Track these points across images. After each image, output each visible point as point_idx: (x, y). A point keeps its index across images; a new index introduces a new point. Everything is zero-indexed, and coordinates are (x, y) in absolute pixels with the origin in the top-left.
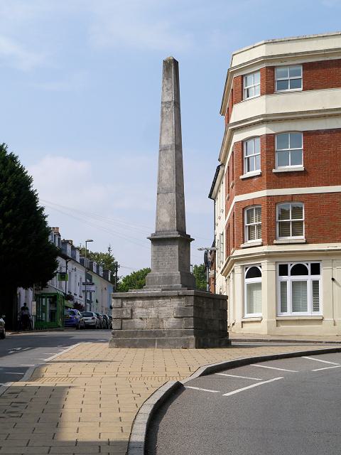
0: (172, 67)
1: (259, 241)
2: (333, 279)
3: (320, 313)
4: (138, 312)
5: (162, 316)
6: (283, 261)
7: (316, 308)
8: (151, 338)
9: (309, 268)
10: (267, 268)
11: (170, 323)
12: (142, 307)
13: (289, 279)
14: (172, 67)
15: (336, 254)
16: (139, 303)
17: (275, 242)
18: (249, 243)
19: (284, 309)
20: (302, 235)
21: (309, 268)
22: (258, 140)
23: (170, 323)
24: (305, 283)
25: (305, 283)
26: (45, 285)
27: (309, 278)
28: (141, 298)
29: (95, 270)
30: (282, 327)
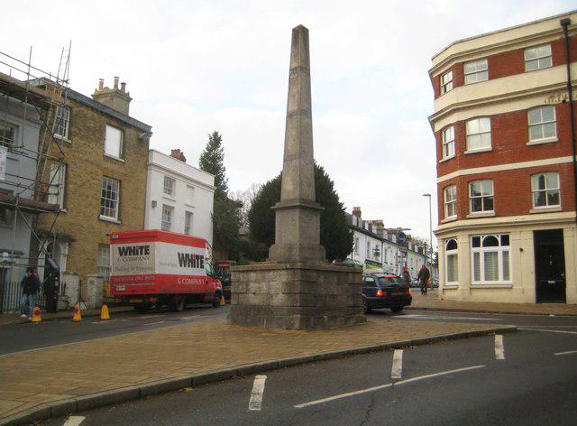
0: (301, 36)
2: (521, 250)
3: (510, 282)
4: (253, 286)
5: (272, 292)
7: (506, 276)
9: (499, 239)
10: (463, 241)
11: (279, 299)
12: (255, 282)
13: (482, 250)
14: (301, 36)
15: (570, 223)
16: (253, 275)
17: (468, 216)
18: (448, 218)
19: (477, 278)
20: (557, 203)
21: (499, 239)
22: (452, 128)
23: (279, 299)
24: (496, 253)
25: (496, 253)
26: (344, 257)
27: (500, 249)
29: (410, 248)
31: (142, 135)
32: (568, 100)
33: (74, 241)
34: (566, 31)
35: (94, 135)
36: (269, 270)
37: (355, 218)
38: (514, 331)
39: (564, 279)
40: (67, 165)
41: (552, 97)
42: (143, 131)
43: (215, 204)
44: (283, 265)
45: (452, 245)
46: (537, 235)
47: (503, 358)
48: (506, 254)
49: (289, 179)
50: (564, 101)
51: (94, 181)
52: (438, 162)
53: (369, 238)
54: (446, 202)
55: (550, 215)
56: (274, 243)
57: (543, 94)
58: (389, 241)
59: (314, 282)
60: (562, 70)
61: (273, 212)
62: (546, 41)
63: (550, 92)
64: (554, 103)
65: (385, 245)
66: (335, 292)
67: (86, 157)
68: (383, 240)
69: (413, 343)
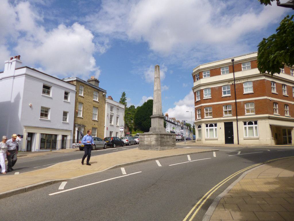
1: (211, 117)
2: (220, 128)
3: (217, 137)
4: (146, 139)
6: (207, 123)
8: (148, 147)
11: (154, 143)
16: (146, 136)
21: (214, 125)
24: (213, 129)
25: (213, 129)
28: (146, 135)
30: (207, 141)
31: (104, 93)
32: (234, 83)
33: (85, 126)
34: (233, 63)
35: (90, 94)
36: (151, 135)
37: (166, 117)
38: (218, 151)
39: (233, 137)
40: (83, 103)
41: (229, 82)
42: (104, 92)
43: (24, 85)
44: (155, 133)
45: (200, 127)
46: (225, 123)
47: (215, 156)
48: (216, 129)
49: (155, 109)
50: (233, 84)
51: (91, 108)
52: (195, 101)
53: (171, 124)
54: (197, 113)
55: (229, 117)
56: (151, 127)
57: (227, 81)
58: (177, 125)
59: (163, 138)
60: (232, 74)
61: (151, 118)
62: (227, 65)
63: (229, 81)
64: (230, 84)
65: (176, 126)
66: (169, 140)
67: (88, 101)
68: (175, 124)
69: (192, 153)
